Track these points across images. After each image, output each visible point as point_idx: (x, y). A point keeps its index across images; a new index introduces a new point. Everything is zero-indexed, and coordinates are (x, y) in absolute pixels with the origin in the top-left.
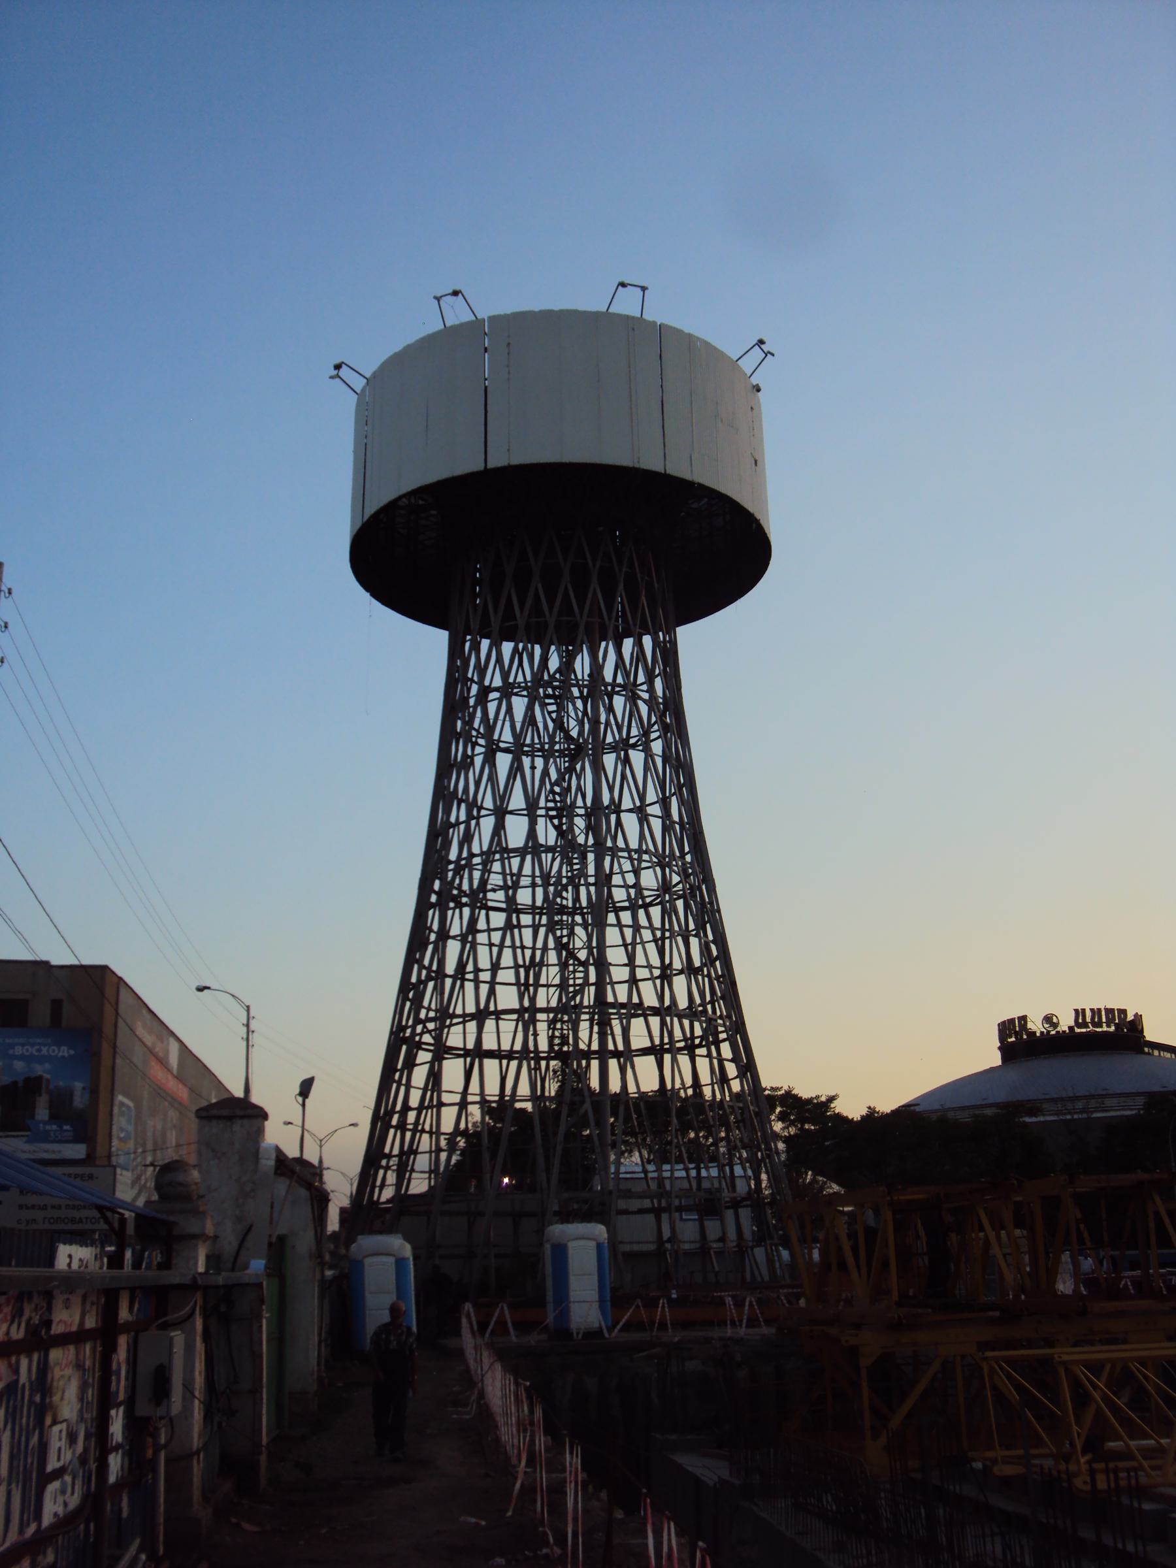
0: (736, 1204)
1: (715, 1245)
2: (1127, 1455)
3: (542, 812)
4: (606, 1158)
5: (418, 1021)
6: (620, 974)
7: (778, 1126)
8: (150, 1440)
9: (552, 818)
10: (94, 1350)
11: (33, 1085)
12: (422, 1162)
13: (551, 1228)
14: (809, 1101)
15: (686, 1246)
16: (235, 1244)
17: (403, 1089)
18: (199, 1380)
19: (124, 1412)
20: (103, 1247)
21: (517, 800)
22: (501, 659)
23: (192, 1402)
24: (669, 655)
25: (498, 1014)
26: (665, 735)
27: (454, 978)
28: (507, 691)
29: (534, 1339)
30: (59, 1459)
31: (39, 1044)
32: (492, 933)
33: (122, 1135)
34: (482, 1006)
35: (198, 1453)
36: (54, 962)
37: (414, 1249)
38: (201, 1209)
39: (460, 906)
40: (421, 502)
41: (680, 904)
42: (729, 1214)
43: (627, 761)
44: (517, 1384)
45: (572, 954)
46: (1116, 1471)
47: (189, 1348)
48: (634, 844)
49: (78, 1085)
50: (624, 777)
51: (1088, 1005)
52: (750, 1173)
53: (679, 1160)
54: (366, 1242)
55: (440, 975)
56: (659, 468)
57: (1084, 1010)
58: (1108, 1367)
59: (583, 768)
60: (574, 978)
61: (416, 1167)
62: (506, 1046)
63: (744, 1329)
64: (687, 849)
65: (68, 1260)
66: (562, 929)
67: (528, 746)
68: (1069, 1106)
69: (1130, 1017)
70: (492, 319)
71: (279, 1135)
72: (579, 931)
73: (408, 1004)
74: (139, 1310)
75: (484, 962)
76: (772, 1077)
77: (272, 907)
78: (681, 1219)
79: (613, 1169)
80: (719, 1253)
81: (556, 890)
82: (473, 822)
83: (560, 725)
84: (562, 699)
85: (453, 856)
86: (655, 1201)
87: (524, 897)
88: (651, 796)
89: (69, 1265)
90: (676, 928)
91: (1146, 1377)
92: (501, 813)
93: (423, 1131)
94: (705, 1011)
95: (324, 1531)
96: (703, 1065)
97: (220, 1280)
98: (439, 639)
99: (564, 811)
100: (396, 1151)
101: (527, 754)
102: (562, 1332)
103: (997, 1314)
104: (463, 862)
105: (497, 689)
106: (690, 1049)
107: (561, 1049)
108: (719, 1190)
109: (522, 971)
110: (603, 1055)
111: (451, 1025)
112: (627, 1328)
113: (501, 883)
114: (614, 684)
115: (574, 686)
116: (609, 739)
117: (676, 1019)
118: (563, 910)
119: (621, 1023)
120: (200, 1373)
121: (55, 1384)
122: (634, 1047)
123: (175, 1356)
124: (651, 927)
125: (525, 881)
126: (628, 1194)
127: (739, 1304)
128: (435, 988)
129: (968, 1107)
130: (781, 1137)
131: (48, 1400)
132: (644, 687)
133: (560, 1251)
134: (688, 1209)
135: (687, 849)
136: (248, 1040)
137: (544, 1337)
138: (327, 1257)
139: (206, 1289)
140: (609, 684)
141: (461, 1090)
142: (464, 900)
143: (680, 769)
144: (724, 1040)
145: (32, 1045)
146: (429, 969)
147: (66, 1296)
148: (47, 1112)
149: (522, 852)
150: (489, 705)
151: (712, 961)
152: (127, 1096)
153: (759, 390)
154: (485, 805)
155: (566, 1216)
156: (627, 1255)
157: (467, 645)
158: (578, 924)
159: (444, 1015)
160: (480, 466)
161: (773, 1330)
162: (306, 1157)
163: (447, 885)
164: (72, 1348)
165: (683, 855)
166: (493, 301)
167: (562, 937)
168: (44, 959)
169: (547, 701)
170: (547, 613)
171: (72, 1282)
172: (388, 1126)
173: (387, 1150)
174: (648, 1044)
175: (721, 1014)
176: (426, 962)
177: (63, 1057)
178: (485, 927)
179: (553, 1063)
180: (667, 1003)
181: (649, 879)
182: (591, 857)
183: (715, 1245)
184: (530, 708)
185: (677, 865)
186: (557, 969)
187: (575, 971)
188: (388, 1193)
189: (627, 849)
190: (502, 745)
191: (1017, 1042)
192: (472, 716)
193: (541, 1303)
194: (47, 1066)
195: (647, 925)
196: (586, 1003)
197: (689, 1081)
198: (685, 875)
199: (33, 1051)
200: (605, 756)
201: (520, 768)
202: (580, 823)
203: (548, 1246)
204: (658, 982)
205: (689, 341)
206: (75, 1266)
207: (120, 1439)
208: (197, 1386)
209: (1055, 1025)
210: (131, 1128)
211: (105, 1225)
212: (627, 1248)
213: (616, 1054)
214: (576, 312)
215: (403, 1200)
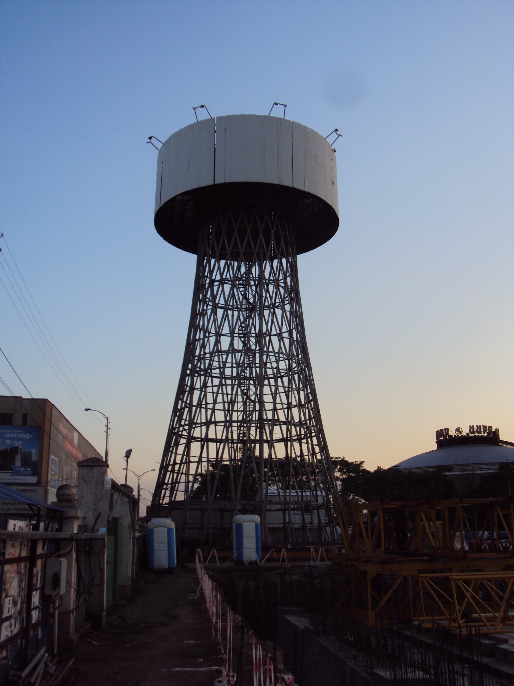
0: (318, 508)
2: (479, 620)
3: (237, 335)
4: (261, 486)
5: (181, 425)
6: (269, 406)
7: (338, 474)
8: (52, 605)
9: (241, 338)
10: (25, 566)
11: (14, 450)
12: (182, 487)
13: (235, 517)
14: (352, 463)
15: (297, 526)
16: (93, 521)
17: (173, 455)
18: (74, 579)
20: (30, 521)
21: (226, 330)
22: (219, 268)
23: (71, 589)
24: (294, 267)
25: (216, 423)
27: (197, 407)
28: (222, 282)
29: (227, 565)
30: (9, 612)
31: (18, 433)
33: (53, 473)
35: (73, 611)
36: (24, 397)
37: (175, 524)
38: (76, 506)
39: (200, 375)
40: (186, 198)
41: (296, 376)
43: (274, 313)
44: (213, 584)
45: (248, 398)
46: (470, 627)
47: (69, 566)
48: (277, 350)
49: (34, 451)
50: (273, 321)
51: (475, 424)
53: (294, 488)
54: (155, 521)
55: (191, 405)
56: (290, 185)
57: (473, 426)
58: (474, 582)
59: (255, 315)
60: (249, 408)
61: (179, 489)
62: (219, 437)
63: (318, 562)
65: (14, 527)
66: (244, 386)
67: (231, 306)
68: (466, 467)
69: (494, 430)
70: (218, 118)
71: (116, 473)
72: (252, 387)
73: (176, 418)
74: (47, 549)
75: (210, 399)
76: (334, 453)
77: (118, 374)
78: (295, 514)
80: (310, 529)
81: (242, 369)
82: (206, 339)
83: (245, 297)
84: (247, 285)
85: (197, 354)
87: (228, 372)
88: (284, 329)
89: (14, 529)
90: (294, 387)
91: (491, 588)
92: (218, 335)
93: (182, 473)
94: (306, 423)
95: (128, 645)
96: (305, 447)
97: (83, 537)
98: (193, 258)
99: (246, 335)
100: (170, 482)
101: (230, 309)
102: (240, 562)
103: (427, 558)
104: (202, 356)
105: (218, 281)
106: (299, 440)
110: (261, 442)
111: (195, 427)
112: (268, 560)
113: (218, 366)
114: (269, 280)
115: (252, 280)
116: (266, 304)
117: (293, 427)
118: (245, 378)
119: (269, 428)
120: (74, 576)
121: (7, 580)
122: (274, 439)
123: (62, 569)
124: (283, 386)
125: (228, 365)
126: (271, 503)
127: (317, 551)
128: (188, 411)
129: (422, 468)
130: (340, 479)
131: (3, 587)
132: (282, 281)
133: (240, 527)
134: (297, 509)
135: (299, 353)
136: (107, 432)
137: (232, 564)
138: (137, 527)
139: (77, 540)
140: (267, 280)
141: (198, 456)
142: (202, 373)
143: (297, 319)
144: (314, 436)
145: (14, 433)
146: (186, 403)
147: (12, 542)
148: (20, 462)
149: (227, 352)
150: (214, 287)
151: (310, 402)
152: (55, 456)
153: (335, 151)
154: (212, 332)
155: (244, 511)
157: (205, 261)
158: (251, 384)
159: (192, 423)
160: (211, 183)
163: (194, 367)
164: (15, 565)
166: (219, 110)
167: (244, 390)
168: (17, 395)
169: (240, 286)
170: (240, 246)
171: (14, 536)
172: (166, 471)
173: (166, 481)
174: (281, 437)
176: (185, 400)
177: (27, 438)
178: (211, 385)
179: (239, 445)
181: (283, 365)
182: (257, 355)
184: (232, 289)
186: (242, 404)
187: (249, 405)
188: (167, 500)
189: (274, 352)
190: (220, 305)
191: (444, 440)
192: (207, 292)
193: (231, 548)
194: (20, 442)
195: (282, 385)
196: (254, 419)
197: (298, 453)
198: (299, 364)
199: (15, 436)
201: (227, 316)
202: (253, 340)
203: (234, 524)
204: (286, 410)
205: (304, 130)
206: (17, 529)
207: (38, 604)
209: (461, 433)
210: (57, 470)
211: (33, 513)
213: (267, 441)
214: (255, 115)
215: (173, 503)
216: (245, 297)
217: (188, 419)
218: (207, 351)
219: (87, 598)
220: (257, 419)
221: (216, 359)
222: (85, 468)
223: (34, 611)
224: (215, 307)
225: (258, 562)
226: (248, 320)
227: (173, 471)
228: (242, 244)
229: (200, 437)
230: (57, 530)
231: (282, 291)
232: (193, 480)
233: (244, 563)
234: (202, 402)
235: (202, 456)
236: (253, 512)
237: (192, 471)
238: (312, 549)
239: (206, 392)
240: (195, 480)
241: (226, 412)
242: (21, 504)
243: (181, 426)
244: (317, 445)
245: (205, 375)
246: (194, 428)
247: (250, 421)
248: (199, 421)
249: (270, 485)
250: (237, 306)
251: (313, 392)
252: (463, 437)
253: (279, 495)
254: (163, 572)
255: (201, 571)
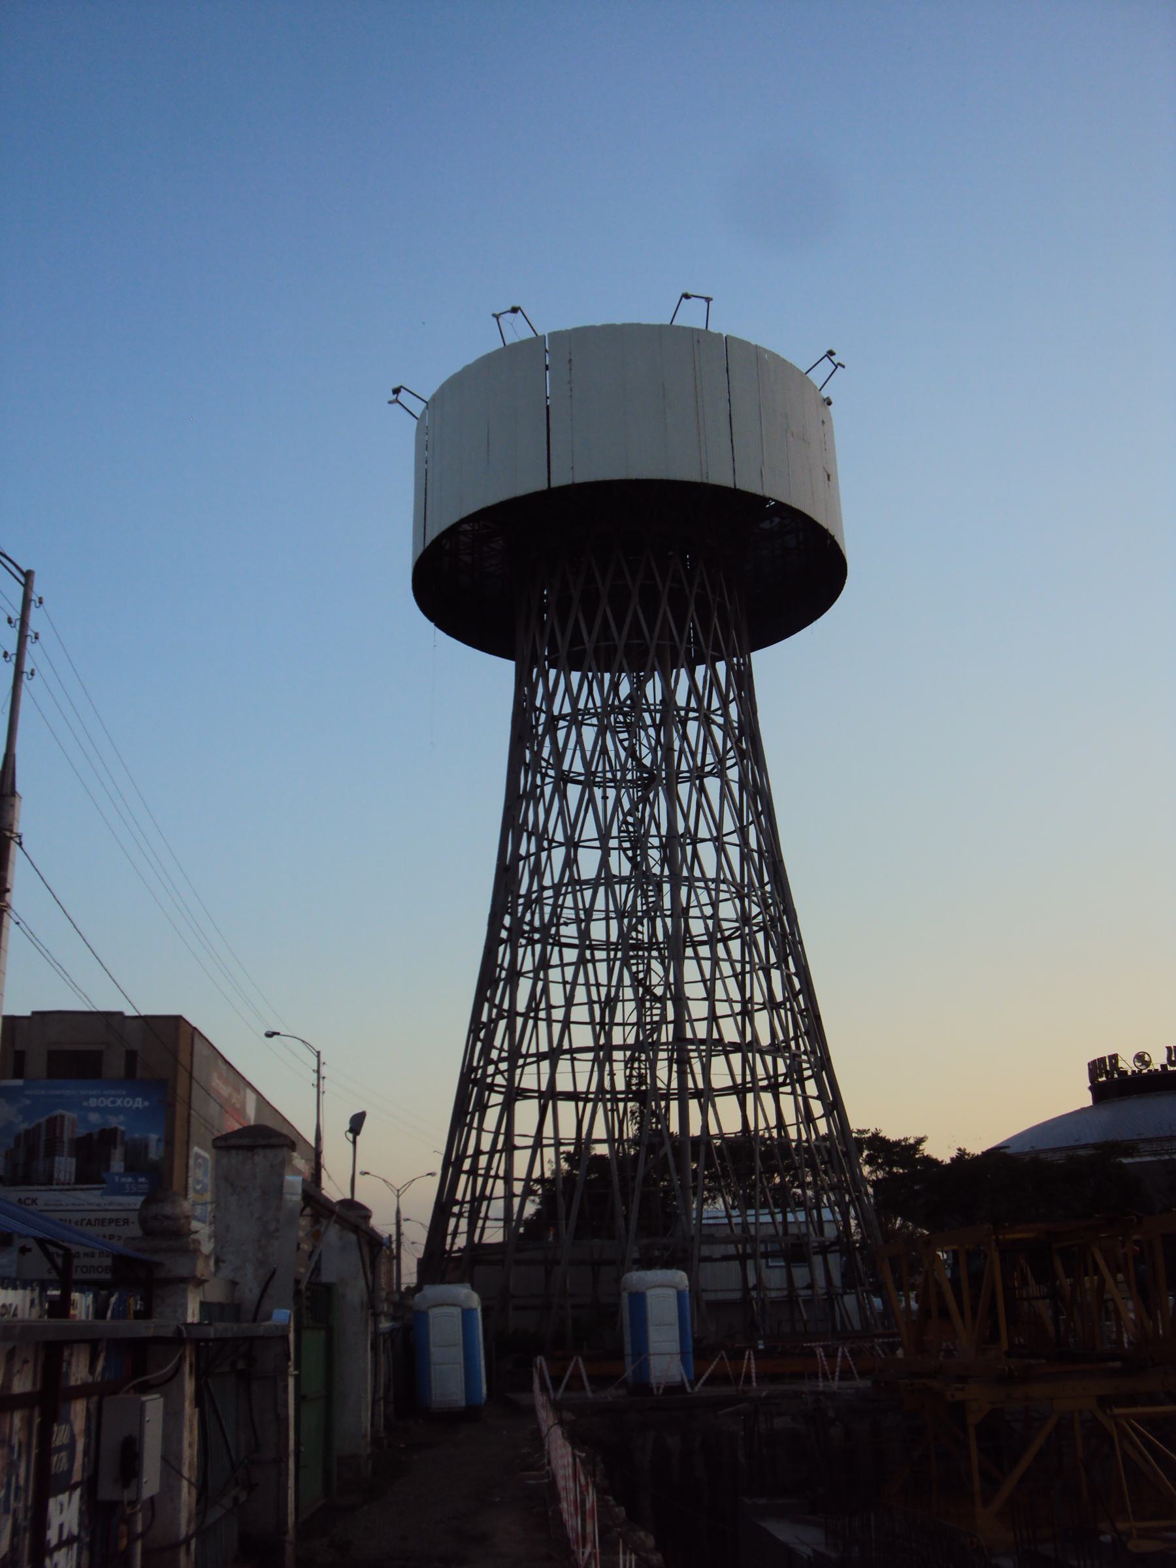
0: (824, 1250)
1: (802, 1293)
5: (490, 1061)
6: (699, 1009)
7: (866, 1170)
8: (123, 1528)
10: (28, 1422)
11: (108, 1137)
14: (897, 1143)
15: (773, 1294)
16: (257, 1292)
17: (474, 1132)
18: (189, 1452)
19: (81, 1497)
20: (43, 1290)
21: (590, 831)
22: (567, 688)
24: (743, 680)
26: (742, 761)
28: (576, 719)
29: (611, 1394)
32: (566, 969)
33: (199, 1187)
34: (555, 1045)
35: (187, 1541)
39: (531, 942)
41: (760, 937)
42: (817, 1260)
43: (702, 790)
44: (574, 1457)
45: (648, 990)
47: (172, 1416)
48: (711, 873)
49: (153, 1137)
50: (699, 806)
52: (839, 1217)
53: (765, 1205)
54: (433, 1291)
59: (657, 795)
60: (652, 1015)
61: (490, 1214)
64: (766, 879)
66: (637, 964)
70: (554, 335)
72: (656, 965)
73: (479, 1045)
75: (557, 995)
76: (860, 1120)
78: (768, 1266)
79: (694, 1215)
81: (630, 922)
82: (544, 855)
83: (632, 753)
84: (632, 729)
85: (523, 891)
86: (740, 1246)
87: (597, 931)
88: (729, 825)
92: (572, 844)
93: (496, 1177)
94: (788, 1047)
96: (787, 1103)
97: (212, 1333)
98: (504, 670)
100: (468, 1198)
102: (642, 1387)
103: (1118, 1364)
106: (774, 1088)
107: (638, 1089)
108: (807, 1235)
109: (597, 1007)
110: (683, 1095)
111: (525, 1065)
112: (711, 1381)
113: (573, 917)
114: (688, 709)
115: (645, 711)
116: (684, 767)
117: (758, 1056)
118: (638, 946)
120: (191, 1445)
126: (711, 1240)
127: (831, 1355)
133: (638, 1299)
135: (766, 879)
140: (682, 709)
141: (533, 1132)
142: (537, 936)
143: (757, 794)
144: (809, 1078)
145: (107, 1097)
148: (122, 1164)
149: (594, 884)
153: (829, 403)
154: (556, 838)
155: (647, 1263)
156: (711, 1305)
159: (514, 1054)
160: (543, 486)
161: (869, 1383)
162: (357, 1198)
163: (518, 922)
165: (762, 885)
167: (638, 972)
173: (459, 1196)
174: (730, 1083)
175: (805, 1049)
176: (497, 1002)
179: (630, 1104)
180: (749, 1038)
181: (728, 910)
182: (666, 887)
183: (802, 1293)
185: (756, 896)
186: (633, 1005)
187: (651, 1008)
188: (461, 1241)
189: (704, 879)
191: (1109, 1081)
192: (541, 746)
193: (619, 1355)
194: (122, 1118)
196: (663, 1039)
197: (773, 1122)
198: (764, 906)
199: (107, 1102)
200: (679, 786)
202: (655, 854)
203: (625, 1295)
204: (739, 1018)
205: (756, 354)
207: (75, 1531)
208: (186, 1462)
212: (711, 1297)
213: (697, 1094)
215: (477, 1251)
216: (632, 753)
217: (506, 1047)
218: (547, 882)
219: (243, 1497)
220: (670, 1040)
221: (569, 901)
222: (234, 1152)
223: (64, 1550)
224: (563, 779)
225: (687, 1385)
226: (640, 806)
227: (473, 1172)
228: (620, 628)
229: (536, 1088)
230: (138, 1315)
231: (718, 734)
232: (524, 1191)
233: (652, 1389)
234: (538, 1004)
235: (545, 1133)
236: (668, 1264)
237: (520, 1170)
238: (820, 1351)
239: (546, 982)
240: (528, 1192)
241: (598, 1027)
242: (93, 1255)
243: (491, 1062)
244: (817, 1098)
245: (543, 942)
246: (523, 1066)
247: (655, 1046)
248: (533, 1050)
249: (705, 1200)
250: (614, 776)
251: (803, 972)
252: (1153, 1074)
253: (730, 1223)
254: (453, 1418)
255: (546, 1417)
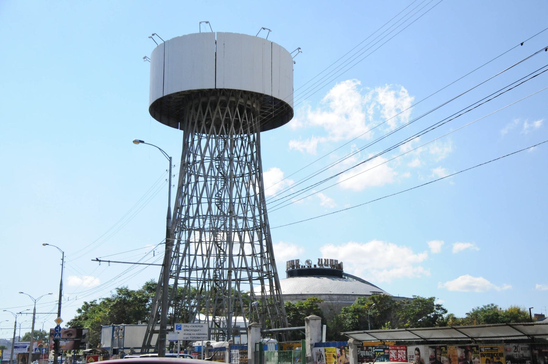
51: (324, 258)
57: (322, 259)
69: (339, 263)
70: (218, 33)
75: (193, 252)
98: (180, 133)
99: (220, 202)
136: (62, 265)
209: (309, 264)
